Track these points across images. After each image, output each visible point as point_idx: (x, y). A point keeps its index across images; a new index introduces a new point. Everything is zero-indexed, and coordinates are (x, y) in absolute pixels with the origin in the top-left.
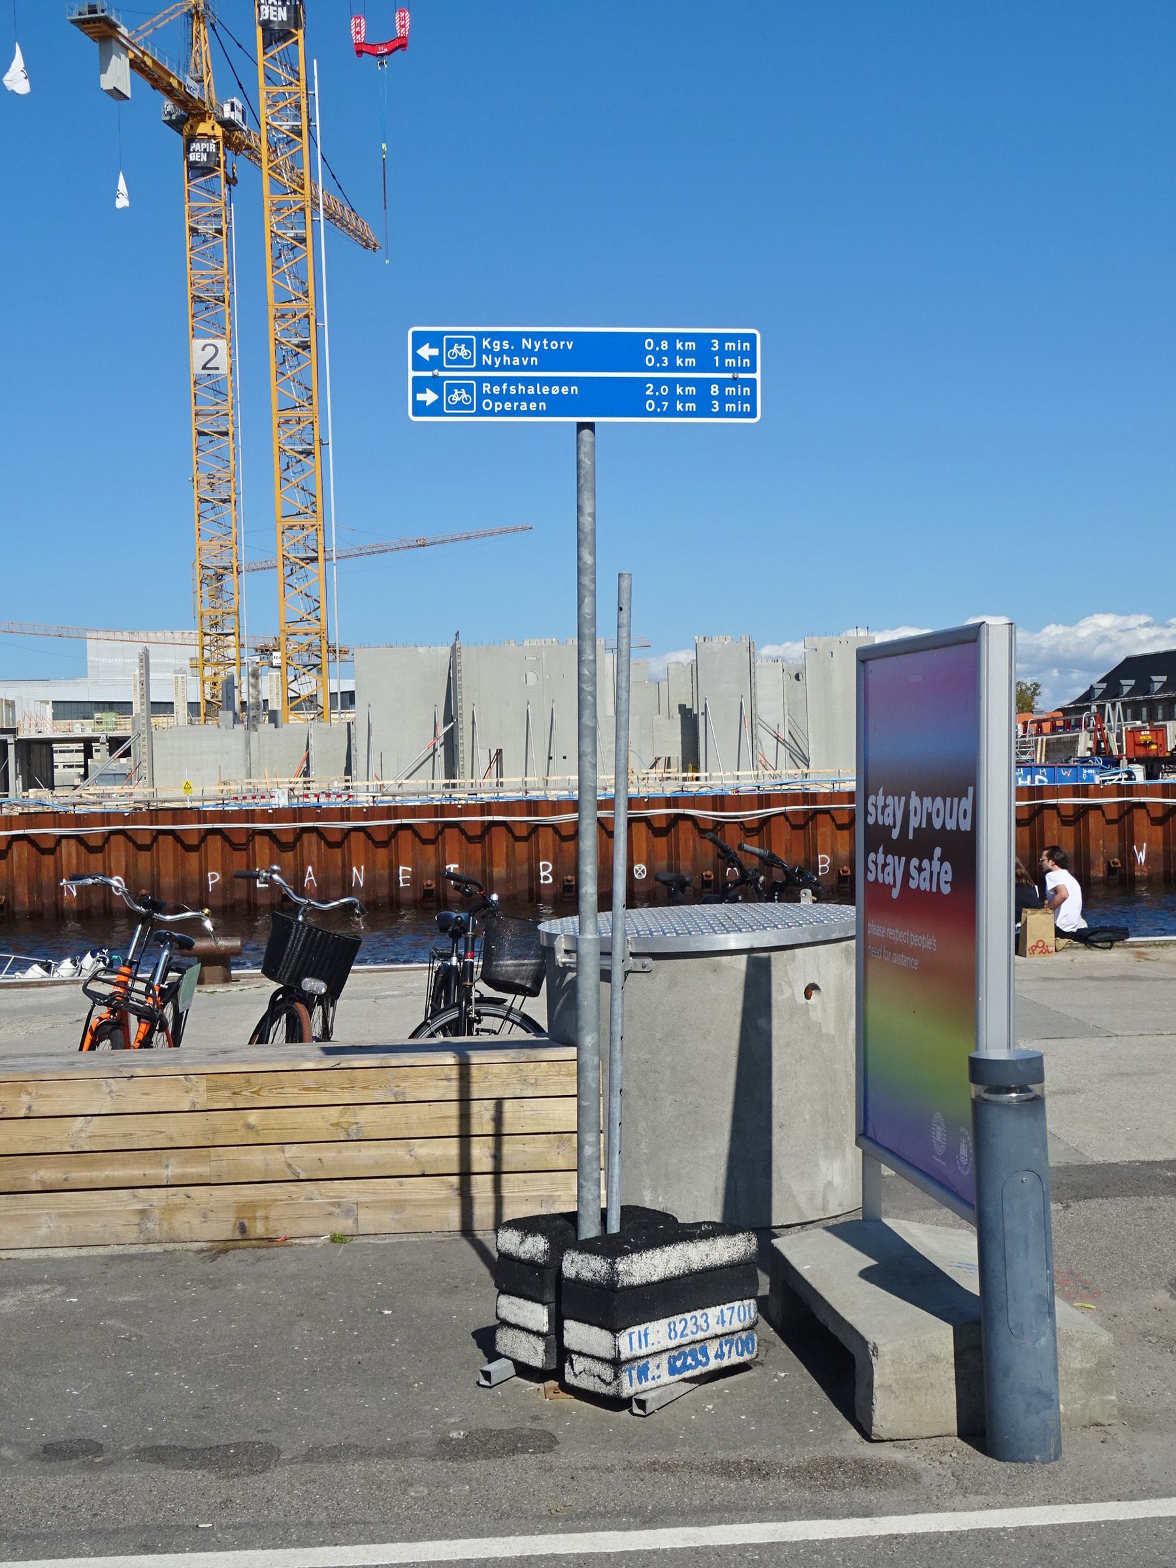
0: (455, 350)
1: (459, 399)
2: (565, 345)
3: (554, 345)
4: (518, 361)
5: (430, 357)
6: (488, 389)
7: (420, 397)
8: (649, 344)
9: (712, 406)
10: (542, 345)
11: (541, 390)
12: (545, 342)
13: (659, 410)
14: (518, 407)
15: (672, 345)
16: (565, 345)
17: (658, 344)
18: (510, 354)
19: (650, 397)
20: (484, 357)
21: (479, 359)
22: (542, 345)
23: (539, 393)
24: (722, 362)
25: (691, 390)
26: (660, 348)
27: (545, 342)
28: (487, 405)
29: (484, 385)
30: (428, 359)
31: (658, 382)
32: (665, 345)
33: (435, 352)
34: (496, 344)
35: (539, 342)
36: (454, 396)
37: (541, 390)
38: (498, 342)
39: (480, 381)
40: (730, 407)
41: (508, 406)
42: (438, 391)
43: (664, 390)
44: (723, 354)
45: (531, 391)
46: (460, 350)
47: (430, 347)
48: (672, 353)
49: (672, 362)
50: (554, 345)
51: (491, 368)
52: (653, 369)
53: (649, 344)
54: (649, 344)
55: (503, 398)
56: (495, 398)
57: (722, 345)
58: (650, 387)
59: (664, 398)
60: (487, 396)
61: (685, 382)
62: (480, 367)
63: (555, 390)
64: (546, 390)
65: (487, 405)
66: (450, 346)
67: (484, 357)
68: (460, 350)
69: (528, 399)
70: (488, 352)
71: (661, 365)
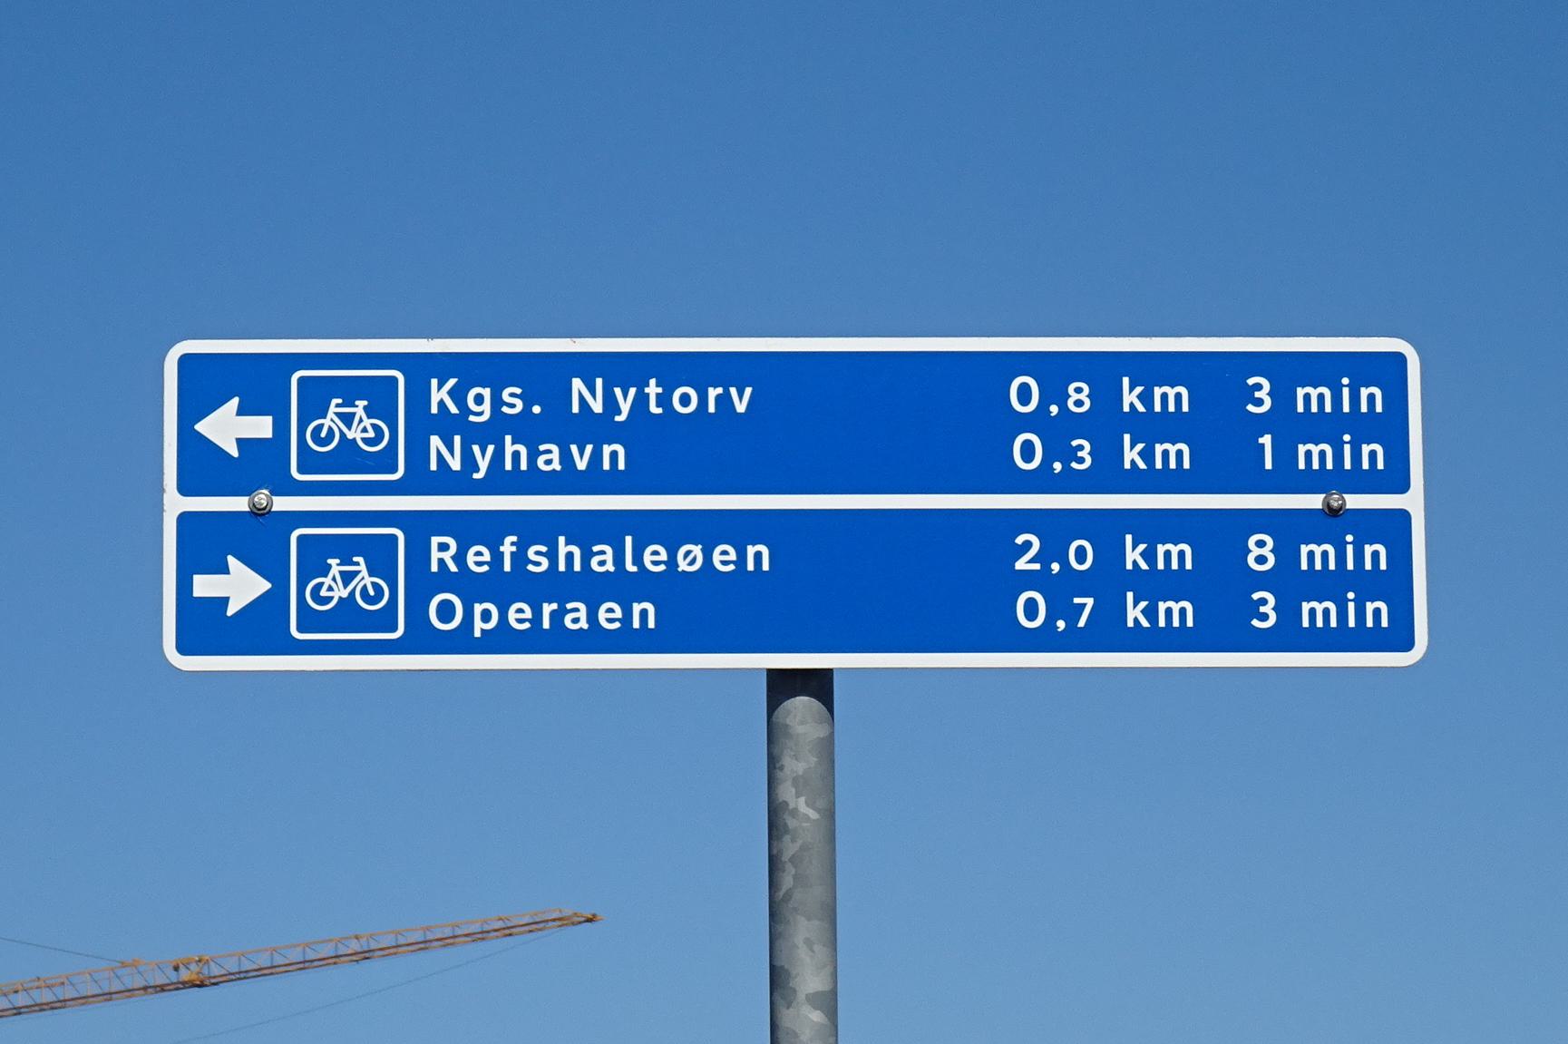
0: (330, 421)
1: (345, 594)
2: (724, 400)
3: (685, 400)
4: (555, 456)
7: (204, 586)
9: (1254, 610)
10: (641, 399)
11: (638, 559)
12: (653, 389)
13: (1054, 409)
14: (557, 616)
16: (724, 400)
17: (1055, 392)
18: (526, 428)
19: (1029, 581)
20: (435, 441)
21: (418, 451)
22: (641, 399)
23: (631, 568)
24: (1285, 453)
25: (1177, 554)
27: (653, 389)
28: (446, 611)
31: (1056, 528)
32: (1079, 396)
33: (261, 427)
34: (479, 399)
35: (632, 391)
36: (328, 581)
37: (638, 559)
38: (486, 392)
39: (420, 526)
40: (1316, 611)
41: (518, 616)
45: (604, 560)
46: (348, 419)
49: (1108, 454)
51: (461, 483)
52: (1044, 640)
54: (1024, 398)
55: (500, 586)
56: (470, 587)
57: (1283, 396)
58: (1028, 545)
60: (444, 580)
61: (1153, 527)
62: (419, 481)
63: (690, 558)
64: (655, 557)
65: (446, 611)
67: (435, 441)
69: (592, 588)
70: (448, 425)
71: (1066, 467)
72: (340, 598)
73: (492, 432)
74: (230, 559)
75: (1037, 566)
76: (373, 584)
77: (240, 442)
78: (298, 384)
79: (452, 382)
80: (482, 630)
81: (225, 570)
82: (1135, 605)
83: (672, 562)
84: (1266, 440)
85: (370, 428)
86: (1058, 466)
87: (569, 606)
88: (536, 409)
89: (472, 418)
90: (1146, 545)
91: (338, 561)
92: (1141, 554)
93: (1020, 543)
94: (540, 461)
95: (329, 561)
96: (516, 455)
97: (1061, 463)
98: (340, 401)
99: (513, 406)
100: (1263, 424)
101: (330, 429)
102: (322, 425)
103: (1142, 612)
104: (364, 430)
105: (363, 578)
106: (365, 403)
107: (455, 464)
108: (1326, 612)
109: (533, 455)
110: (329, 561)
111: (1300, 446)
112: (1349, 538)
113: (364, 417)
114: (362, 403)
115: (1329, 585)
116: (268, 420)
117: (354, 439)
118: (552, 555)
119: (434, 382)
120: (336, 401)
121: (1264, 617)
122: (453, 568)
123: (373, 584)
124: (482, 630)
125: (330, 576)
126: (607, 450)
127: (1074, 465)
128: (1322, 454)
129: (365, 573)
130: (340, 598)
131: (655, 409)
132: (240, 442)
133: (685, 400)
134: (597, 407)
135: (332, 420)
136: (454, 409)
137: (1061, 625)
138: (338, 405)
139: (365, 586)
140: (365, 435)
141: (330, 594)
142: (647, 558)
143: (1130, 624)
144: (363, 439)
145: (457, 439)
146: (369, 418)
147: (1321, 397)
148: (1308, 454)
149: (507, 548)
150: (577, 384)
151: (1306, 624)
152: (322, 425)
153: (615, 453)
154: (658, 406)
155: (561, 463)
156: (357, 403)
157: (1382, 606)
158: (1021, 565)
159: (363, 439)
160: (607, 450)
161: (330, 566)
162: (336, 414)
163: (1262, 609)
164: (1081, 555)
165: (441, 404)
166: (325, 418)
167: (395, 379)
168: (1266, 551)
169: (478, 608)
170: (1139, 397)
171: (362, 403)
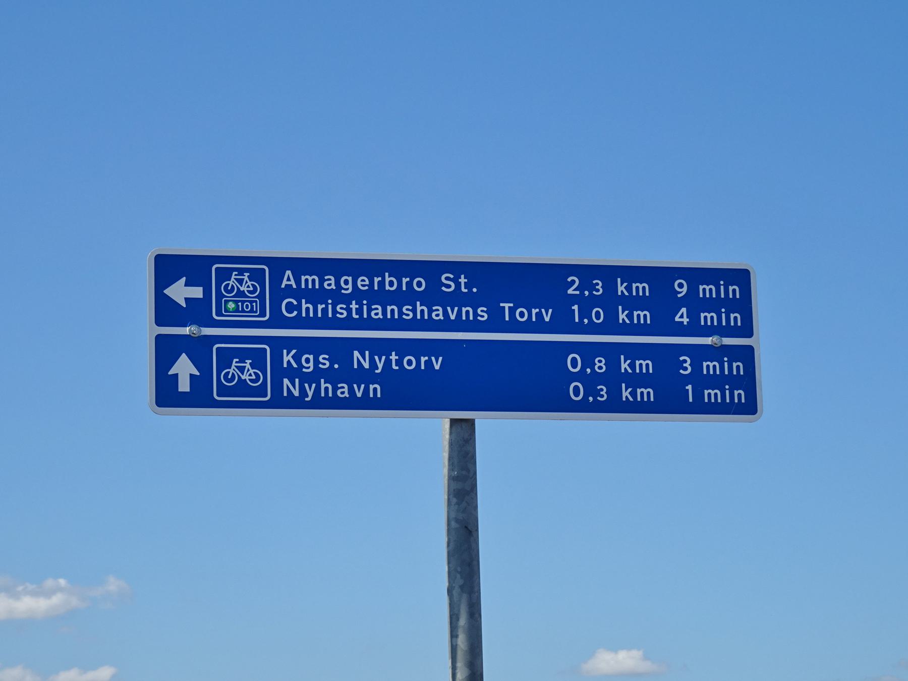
0: (232, 282)
2: (429, 363)
3: (410, 363)
4: (346, 390)
5: (187, 300)
8: (574, 363)
10: (388, 362)
12: (394, 357)
13: (586, 321)
16: (429, 363)
17: (588, 362)
18: (333, 377)
20: (286, 381)
21: (275, 308)
22: (388, 362)
24: (698, 395)
25: (645, 365)
26: (590, 319)
27: (394, 357)
31: (588, 352)
32: (600, 365)
33: (197, 292)
34: (308, 361)
35: (384, 358)
38: (311, 357)
39: (278, 344)
40: (707, 317)
43: (598, 315)
44: (695, 304)
46: (242, 369)
48: (613, 378)
49: (612, 315)
50: (410, 363)
53: (574, 363)
54: (573, 363)
55: (316, 296)
57: (697, 366)
58: (573, 282)
59: (594, 301)
61: (635, 352)
62: (277, 321)
66: (224, 363)
67: (286, 381)
68: (242, 369)
70: (293, 373)
73: (317, 375)
75: (578, 292)
77: (186, 299)
79: (294, 351)
82: (622, 285)
84: (689, 387)
85: (253, 374)
86: (591, 399)
88: (336, 366)
89: (304, 370)
94: (339, 392)
96: (326, 389)
99: (324, 364)
100: (688, 379)
101: (233, 373)
102: (229, 372)
103: (629, 393)
104: (250, 375)
107: (296, 393)
109: (335, 389)
111: (702, 314)
112: (723, 310)
114: (249, 361)
115: (713, 305)
116: (201, 289)
119: (285, 351)
120: (235, 360)
125: (232, 368)
126: (372, 387)
131: (395, 367)
132: (186, 299)
133: (410, 363)
134: (366, 365)
135: (233, 282)
136: (295, 365)
138: (236, 275)
140: (250, 378)
143: (620, 293)
144: (249, 380)
145: (297, 380)
146: (250, 281)
147: (711, 290)
148: (706, 317)
150: (356, 354)
151: (705, 372)
152: (229, 372)
153: (375, 388)
154: (396, 366)
155: (349, 393)
156: (245, 274)
157: (738, 315)
158: (570, 291)
159: (249, 380)
160: (372, 387)
162: (235, 279)
165: (289, 362)
166: (230, 368)
167: (266, 396)
170: (626, 316)
171: (249, 361)
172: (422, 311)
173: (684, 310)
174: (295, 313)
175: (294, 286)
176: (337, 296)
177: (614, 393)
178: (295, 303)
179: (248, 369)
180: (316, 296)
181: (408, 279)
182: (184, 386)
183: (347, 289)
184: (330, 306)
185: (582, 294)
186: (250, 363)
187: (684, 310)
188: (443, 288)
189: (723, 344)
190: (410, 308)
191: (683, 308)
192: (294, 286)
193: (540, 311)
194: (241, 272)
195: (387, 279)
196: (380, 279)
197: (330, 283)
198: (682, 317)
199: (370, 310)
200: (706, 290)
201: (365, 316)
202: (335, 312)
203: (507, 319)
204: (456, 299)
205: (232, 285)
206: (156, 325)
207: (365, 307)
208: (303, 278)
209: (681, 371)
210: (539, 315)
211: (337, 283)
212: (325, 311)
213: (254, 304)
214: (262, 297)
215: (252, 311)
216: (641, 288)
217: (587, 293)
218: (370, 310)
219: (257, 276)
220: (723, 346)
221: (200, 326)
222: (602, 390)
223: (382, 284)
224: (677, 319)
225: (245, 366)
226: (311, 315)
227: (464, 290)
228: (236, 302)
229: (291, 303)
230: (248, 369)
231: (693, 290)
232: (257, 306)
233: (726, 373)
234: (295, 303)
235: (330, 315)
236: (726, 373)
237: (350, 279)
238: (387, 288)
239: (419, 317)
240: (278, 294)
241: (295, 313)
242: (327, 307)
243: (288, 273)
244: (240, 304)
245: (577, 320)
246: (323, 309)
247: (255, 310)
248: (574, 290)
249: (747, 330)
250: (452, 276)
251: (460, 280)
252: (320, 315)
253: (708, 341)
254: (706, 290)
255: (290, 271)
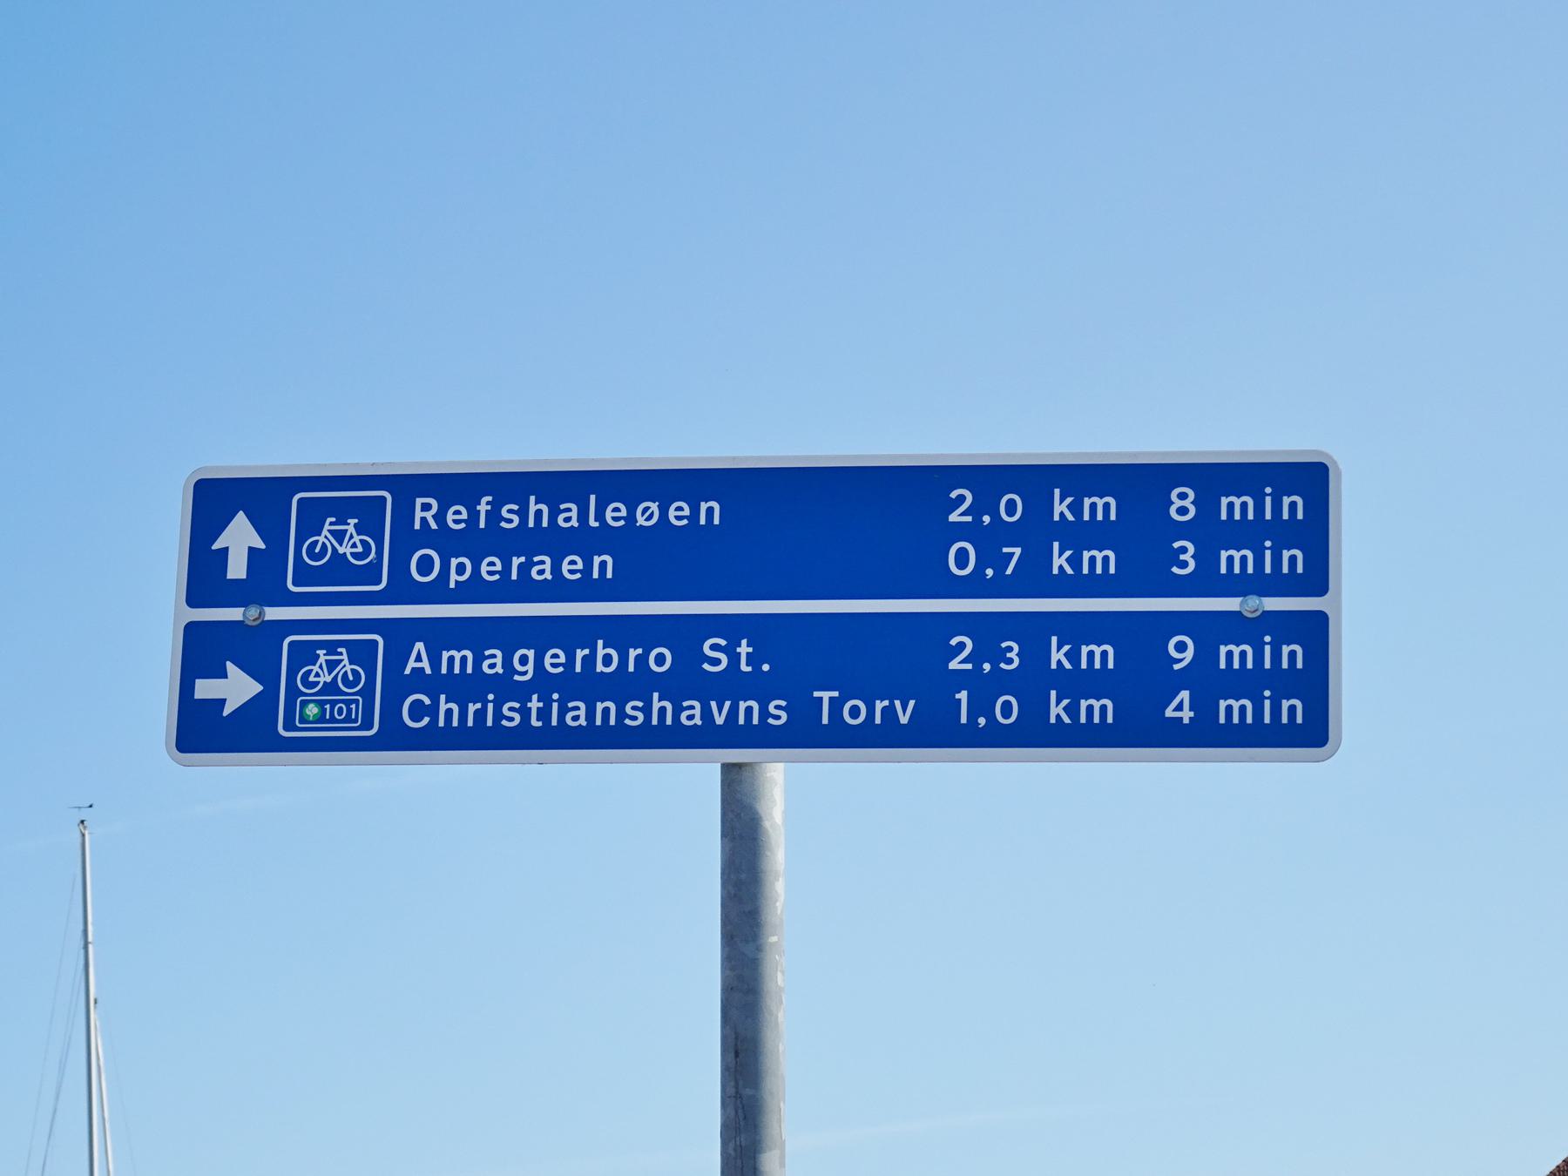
1: (329, 679)
6: (429, 515)
7: (205, 689)
9: (1175, 558)
11: (600, 516)
13: (982, 721)
14: (524, 569)
15: (1035, 654)
19: (960, 531)
23: (593, 523)
25: (1101, 654)
28: (425, 565)
29: (419, 501)
30: (230, 666)
31: (987, 629)
36: (316, 668)
37: (600, 516)
40: (1232, 558)
41: (490, 567)
42: (262, 670)
45: (569, 517)
46: (339, 536)
47: (222, 702)
49: (1037, 560)
51: (438, 592)
52: (973, 587)
55: (474, 542)
56: (449, 543)
58: (962, 646)
59: (1002, 682)
60: (426, 537)
61: (1077, 629)
62: (403, 591)
63: (647, 514)
64: (615, 514)
65: (425, 565)
66: (309, 526)
69: (556, 542)
71: (995, 667)
72: (325, 682)
74: (229, 664)
76: (352, 670)
78: (298, 586)
80: (456, 582)
81: (223, 675)
83: (631, 518)
85: (359, 544)
87: (536, 559)
90: (1070, 646)
91: (325, 652)
92: (1065, 655)
93: (954, 644)
95: (318, 652)
97: (994, 570)
98: (333, 519)
104: (354, 545)
105: (345, 666)
106: (356, 521)
108: (1244, 506)
110: (318, 652)
112: (1267, 639)
113: (355, 534)
114: (353, 521)
117: (345, 553)
118: (523, 513)
121: (1184, 565)
122: (434, 526)
123: (352, 670)
124: (456, 582)
125: (318, 664)
127: (1003, 665)
128: (1243, 709)
129: (346, 662)
130: (325, 682)
135: (326, 537)
137: (990, 572)
138: (331, 524)
139: (346, 672)
140: (354, 550)
141: (317, 679)
142: (609, 514)
146: (358, 534)
148: (1231, 506)
149: (483, 507)
152: (317, 541)
156: (349, 521)
161: (318, 656)
162: (329, 531)
163: (1182, 557)
164: (1011, 508)
166: (320, 535)
168: (1187, 503)
169: (454, 562)
171: (353, 521)
172: (662, 710)
173: (1185, 695)
174: (426, 720)
175: (428, 671)
176: (506, 687)
177: (1035, 708)
178: (427, 701)
179: (351, 534)
180: (465, 687)
181: (639, 651)
182: (237, 569)
183: (525, 673)
184: (490, 706)
185: (978, 520)
186: (355, 525)
187: (1185, 695)
188: (706, 666)
189: (1265, 609)
190: (640, 704)
191: (1183, 692)
192: (428, 671)
193: (892, 705)
194: (331, 647)
195: (601, 652)
196: (587, 651)
197: (494, 662)
198: (1181, 707)
199: (563, 711)
200: (1233, 505)
201: (554, 722)
202: (498, 716)
203: (825, 721)
204: (731, 686)
205: (323, 543)
206: (197, 482)
207: (555, 706)
208: (445, 655)
209: (1175, 570)
210: (889, 712)
211: (507, 662)
212: (479, 715)
213: (353, 706)
214: (368, 692)
215: (348, 719)
216: (1103, 506)
217: (987, 667)
218: (563, 711)
219: (361, 654)
220: (1265, 613)
221: (261, 605)
222: (1010, 649)
223: (589, 661)
224: (1169, 713)
225: (347, 530)
226: (455, 723)
227: (745, 668)
228: (321, 704)
229: (420, 702)
230: (351, 534)
231: (1206, 654)
232: (357, 711)
233: (1267, 720)
234: (427, 701)
235: (490, 723)
236: (1267, 720)
237: (531, 654)
238: (600, 668)
239: (655, 721)
240: (398, 685)
241: (426, 720)
242: (484, 708)
243: (420, 646)
244: (328, 707)
245: (964, 720)
246: (476, 712)
247: (353, 717)
248: (962, 514)
249: (1317, 579)
250: (723, 642)
251: (738, 650)
252: (470, 723)
253: (1230, 604)
254: (1233, 505)
255: (422, 644)
